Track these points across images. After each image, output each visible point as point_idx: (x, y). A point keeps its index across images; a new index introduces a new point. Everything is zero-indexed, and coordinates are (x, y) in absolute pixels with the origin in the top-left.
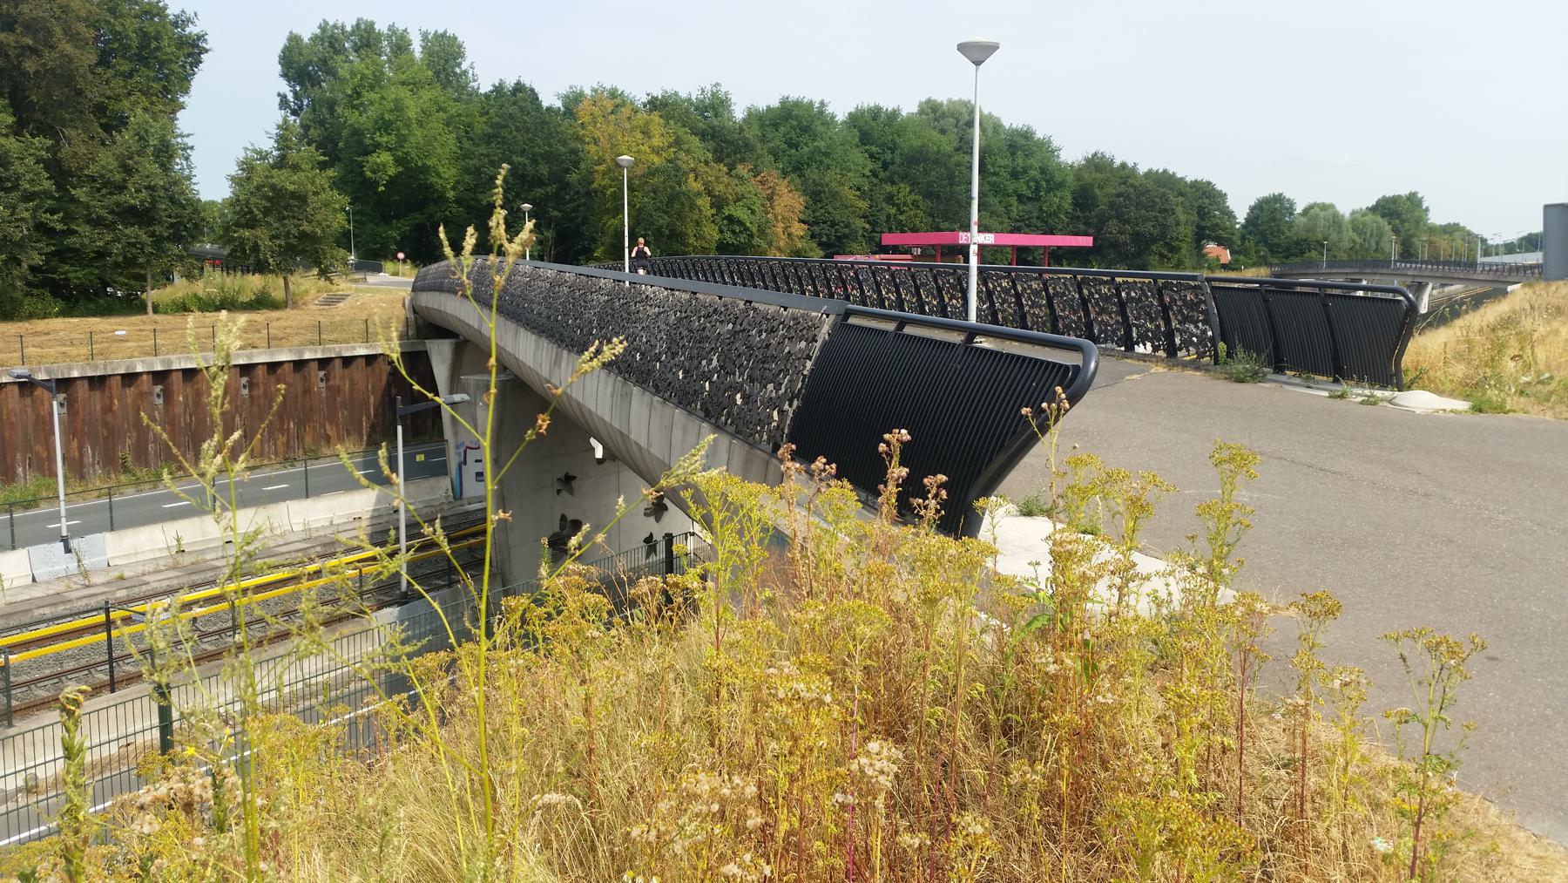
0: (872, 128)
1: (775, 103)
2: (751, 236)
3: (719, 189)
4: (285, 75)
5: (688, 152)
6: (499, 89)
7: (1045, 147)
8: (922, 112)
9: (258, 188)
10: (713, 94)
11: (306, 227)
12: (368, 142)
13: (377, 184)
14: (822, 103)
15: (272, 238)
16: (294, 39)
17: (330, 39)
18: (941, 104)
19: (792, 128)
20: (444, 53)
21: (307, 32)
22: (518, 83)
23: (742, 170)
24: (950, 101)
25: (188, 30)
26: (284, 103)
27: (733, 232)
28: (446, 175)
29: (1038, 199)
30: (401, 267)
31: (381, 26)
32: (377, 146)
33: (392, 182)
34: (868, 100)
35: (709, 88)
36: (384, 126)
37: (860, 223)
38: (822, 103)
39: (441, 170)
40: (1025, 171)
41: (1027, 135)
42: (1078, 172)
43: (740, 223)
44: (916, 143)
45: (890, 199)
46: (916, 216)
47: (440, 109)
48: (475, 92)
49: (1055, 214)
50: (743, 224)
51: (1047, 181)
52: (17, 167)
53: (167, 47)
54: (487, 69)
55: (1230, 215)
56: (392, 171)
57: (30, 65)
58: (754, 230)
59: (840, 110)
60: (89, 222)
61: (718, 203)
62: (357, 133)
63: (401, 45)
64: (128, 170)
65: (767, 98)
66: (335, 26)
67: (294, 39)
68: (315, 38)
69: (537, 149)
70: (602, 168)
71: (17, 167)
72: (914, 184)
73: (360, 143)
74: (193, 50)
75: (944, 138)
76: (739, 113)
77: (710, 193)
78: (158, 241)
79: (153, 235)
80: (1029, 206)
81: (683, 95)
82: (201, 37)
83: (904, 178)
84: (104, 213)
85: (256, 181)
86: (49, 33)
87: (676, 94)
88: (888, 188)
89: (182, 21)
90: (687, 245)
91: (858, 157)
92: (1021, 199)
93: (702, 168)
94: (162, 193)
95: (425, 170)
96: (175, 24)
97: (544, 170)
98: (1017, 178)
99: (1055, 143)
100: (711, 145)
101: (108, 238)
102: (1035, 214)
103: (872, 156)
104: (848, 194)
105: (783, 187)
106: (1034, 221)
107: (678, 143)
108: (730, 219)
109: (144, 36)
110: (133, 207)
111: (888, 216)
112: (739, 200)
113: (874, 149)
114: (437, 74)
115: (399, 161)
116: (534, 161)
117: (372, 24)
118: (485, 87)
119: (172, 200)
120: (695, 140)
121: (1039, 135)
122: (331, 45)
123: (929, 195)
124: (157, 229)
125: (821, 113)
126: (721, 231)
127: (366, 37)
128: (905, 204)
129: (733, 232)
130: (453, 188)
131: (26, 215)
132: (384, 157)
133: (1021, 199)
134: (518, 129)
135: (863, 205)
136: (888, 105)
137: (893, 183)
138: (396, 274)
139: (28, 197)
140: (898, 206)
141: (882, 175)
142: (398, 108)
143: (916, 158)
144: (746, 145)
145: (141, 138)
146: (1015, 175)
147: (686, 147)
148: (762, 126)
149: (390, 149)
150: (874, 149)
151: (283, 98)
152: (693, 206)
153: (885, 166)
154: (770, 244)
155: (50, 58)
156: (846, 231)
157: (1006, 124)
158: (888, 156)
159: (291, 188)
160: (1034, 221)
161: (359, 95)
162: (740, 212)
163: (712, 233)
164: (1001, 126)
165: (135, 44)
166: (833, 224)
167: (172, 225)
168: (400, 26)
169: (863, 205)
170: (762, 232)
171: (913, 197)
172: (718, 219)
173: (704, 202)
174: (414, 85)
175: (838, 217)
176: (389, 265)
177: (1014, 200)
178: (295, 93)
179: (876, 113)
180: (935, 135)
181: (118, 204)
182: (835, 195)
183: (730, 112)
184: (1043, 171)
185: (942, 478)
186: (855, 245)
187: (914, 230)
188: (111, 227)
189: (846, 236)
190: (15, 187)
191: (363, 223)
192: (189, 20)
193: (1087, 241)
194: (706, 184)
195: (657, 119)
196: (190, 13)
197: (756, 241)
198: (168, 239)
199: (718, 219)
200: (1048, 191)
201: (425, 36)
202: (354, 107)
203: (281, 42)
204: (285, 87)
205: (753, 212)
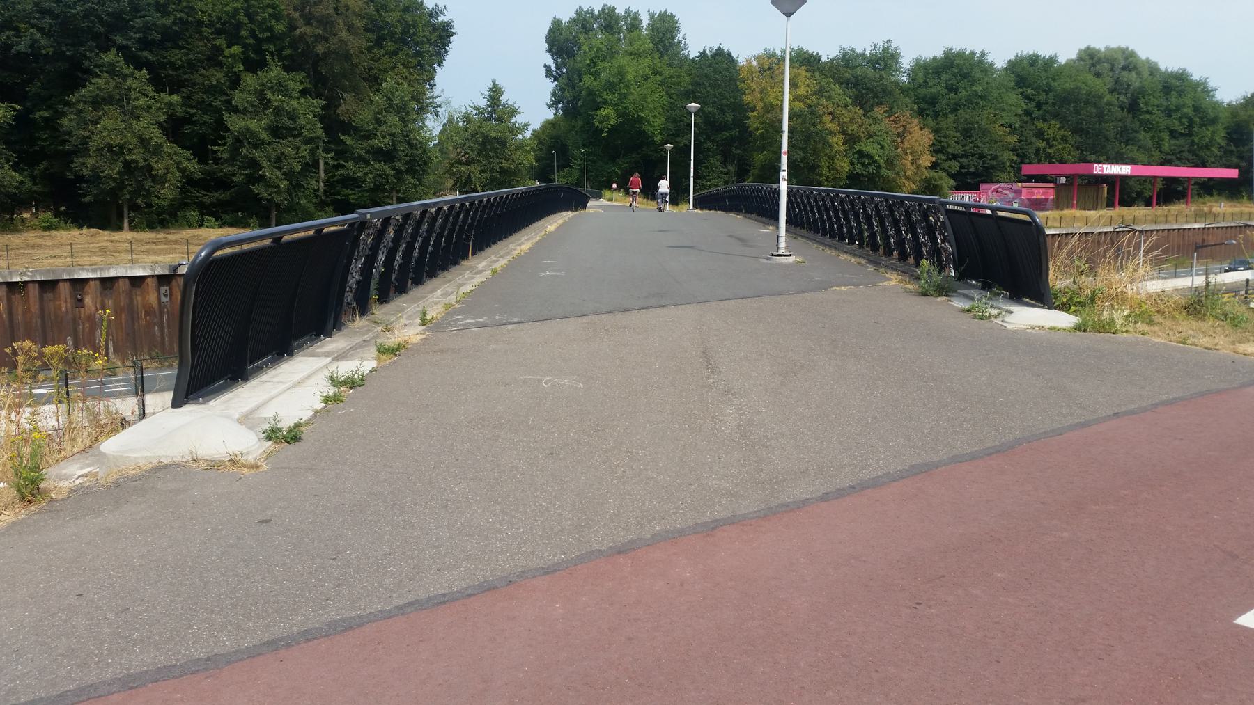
0: (1030, 75)
1: (939, 53)
2: (879, 167)
3: (852, 128)
4: (550, 51)
5: (829, 98)
6: (703, 55)
7: (1201, 89)
8: (1080, 59)
9: (473, 135)
10: (885, 50)
11: (505, 164)
12: (599, 100)
13: (602, 131)
14: (983, 54)
15: (482, 172)
16: (557, 23)
17: (583, 21)
18: (1099, 51)
19: (954, 76)
20: (665, 27)
21: (566, 16)
22: (719, 49)
23: (878, 112)
24: (1108, 48)
25: (440, 19)
26: (549, 73)
27: (863, 164)
28: (656, 124)
29: (1190, 134)
30: (615, 195)
31: (620, 11)
32: (605, 102)
33: (614, 130)
34: (1026, 47)
35: (881, 44)
36: (610, 87)
37: (1007, 156)
38: (983, 54)
39: (652, 119)
40: (1178, 109)
41: (1182, 77)
42: (1233, 110)
43: (869, 156)
44: (1069, 85)
45: (1040, 134)
46: (1064, 149)
47: (655, 73)
48: (687, 57)
49: (1207, 147)
50: (872, 158)
51: (1201, 119)
52: (302, 121)
53: (423, 32)
54: (696, 40)
55: (423, 105)
56: (613, 122)
57: (320, 49)
58: (882, 162)
59: (999, 59)
60: (354, 159)
61: (851, 139)
62: (591, 93)
63: (634, 23)
64: (379, 122)
65: (932, 50)
66: (587, 12)
67: (557, 23)
68: (573, 21)
69: (724, 102)
70: (755, 114)
71: (302, 121)
72: (1064, 122)
73: (594, 101)
74: (443, 34)
75: (1098, 81)
76: (906, 62)
77: (844, 132)
78: (398, 173)
79: (394, 169)
80: (1181, 141)
81: (859, 51)
82: (449, 24)
83: (1055, 116)
84: (362, 152)
85: (471, 128)
86: (332, 24)
87: (853, 50)
88: (1040, 125)
89: (435, 13)
90: (821, 175)
91: (1014, 100)
92: (1173, 134)
93: (839, 111)
94: (401, 139)
95: (640, 120)
96: (431, 15)
97: (729, 117)
98: (1169, 116)
99: (1212, 84)
100: (853, 92)
101: (366, 170)
102: (1186, 148)
103: (1028, 99)
104: (999, 130)
105: (914, 124)
106: (1185, 154)
107: (820, 92)
108: (860, 153)
109: (407, 27)
110: (381, 149)
111: (1038, 150)
112: (871, 137)
113: (1029, 91)
114: (656, 45)
115: (620, 115)
116: (722, 111)
117: (614, 9)
118: (693, 54)
119: (409, 143)
120: (837, 89)
121: (1196, 77)
122: (584, 27)
123: (1077, 131)
124: (398, 165)
125: (981, 61)
126: (852, 164)
127: (608, 19)
128: (1054, 139)
129: (863, 164)
130: (660, 133)
131: (305, 153)
132: (607, 111)
133: (1173, 134)
134: (710, 85)
135: (1013, 140)
136: (1045, 52)
137: (1045, 120)
138: (610, 200)
139: (308, 141)
140: (1047, 140)
141: (1036, 113)
142: (621, 73)
143: (1067, 99)
144: (884, 91)
145: (389, 99)
146: (1169, 113)
147: (827, 94)
148: (926, 74)
149: (613, 105)
150: (1029, 91)
151: (548, 68)
152: (826, 143)
153: (1039, 106)
154: (898, 174)
155: (333, 43)
156: (993, 162)
157: (1162, 67)
158: (1043, 97)
159: (494, 135)
160: (1185, 154)
161: (595, 63)
162: (869, 147)
163: (844, 165)
164: (1158, 69)
165: (399, 30)
166: (981, 156)
167: (407, 162)
168: (633, 9)
169: (1013, 140)
170: (890, 163)
171: (1062, 133)
172: (850, 153)
173: (837, 142)
174: (637, 55)
175: (986, 151)
176: (607, 193)
177: (1166, 136)
178: (556, 64)
179: (1033, 60)
180: (1090, 78)
181: (372, 147)
182: (985, 132)
183: (898, 63)
184: (1197, 109)
185: (86, 200)
186: (1002, 175)
187: (1061, 161)
188: (366, 162)
189: (993, 167)
190: (300, 134)
191: (594, 162)
192: (441, 12)
193: (1233, 173)
194: (841, 125)
195: (804, 73)
196: (441, 6)
197: (883, 171)
198: (407, 172)
199: (850, 153)
200: (1201, 126)
201: (652, 16)
202: (591, 73)
203: (547, 26)
204: (550, 61)
205: (882, 147)
